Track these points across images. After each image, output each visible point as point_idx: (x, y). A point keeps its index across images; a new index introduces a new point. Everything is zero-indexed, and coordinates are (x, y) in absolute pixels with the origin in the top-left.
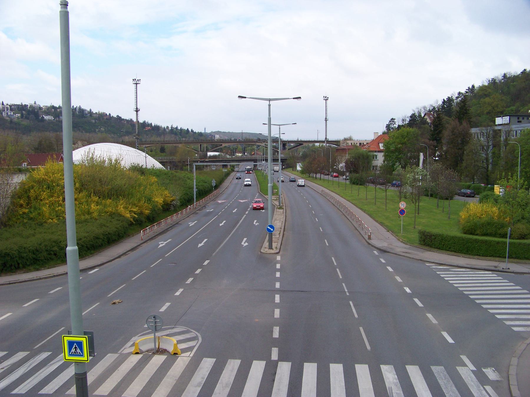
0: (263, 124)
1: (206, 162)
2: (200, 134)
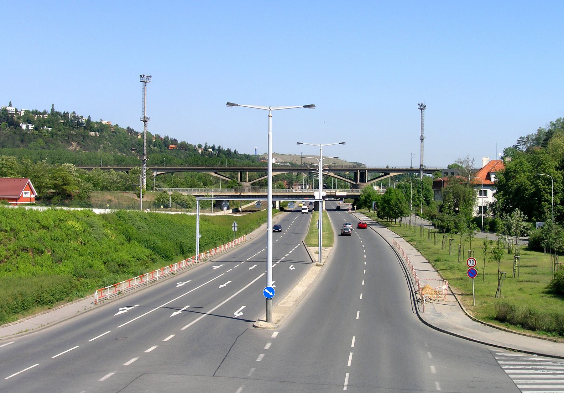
0: (297, 143)
1: (244, 197)
2: (247, 157)
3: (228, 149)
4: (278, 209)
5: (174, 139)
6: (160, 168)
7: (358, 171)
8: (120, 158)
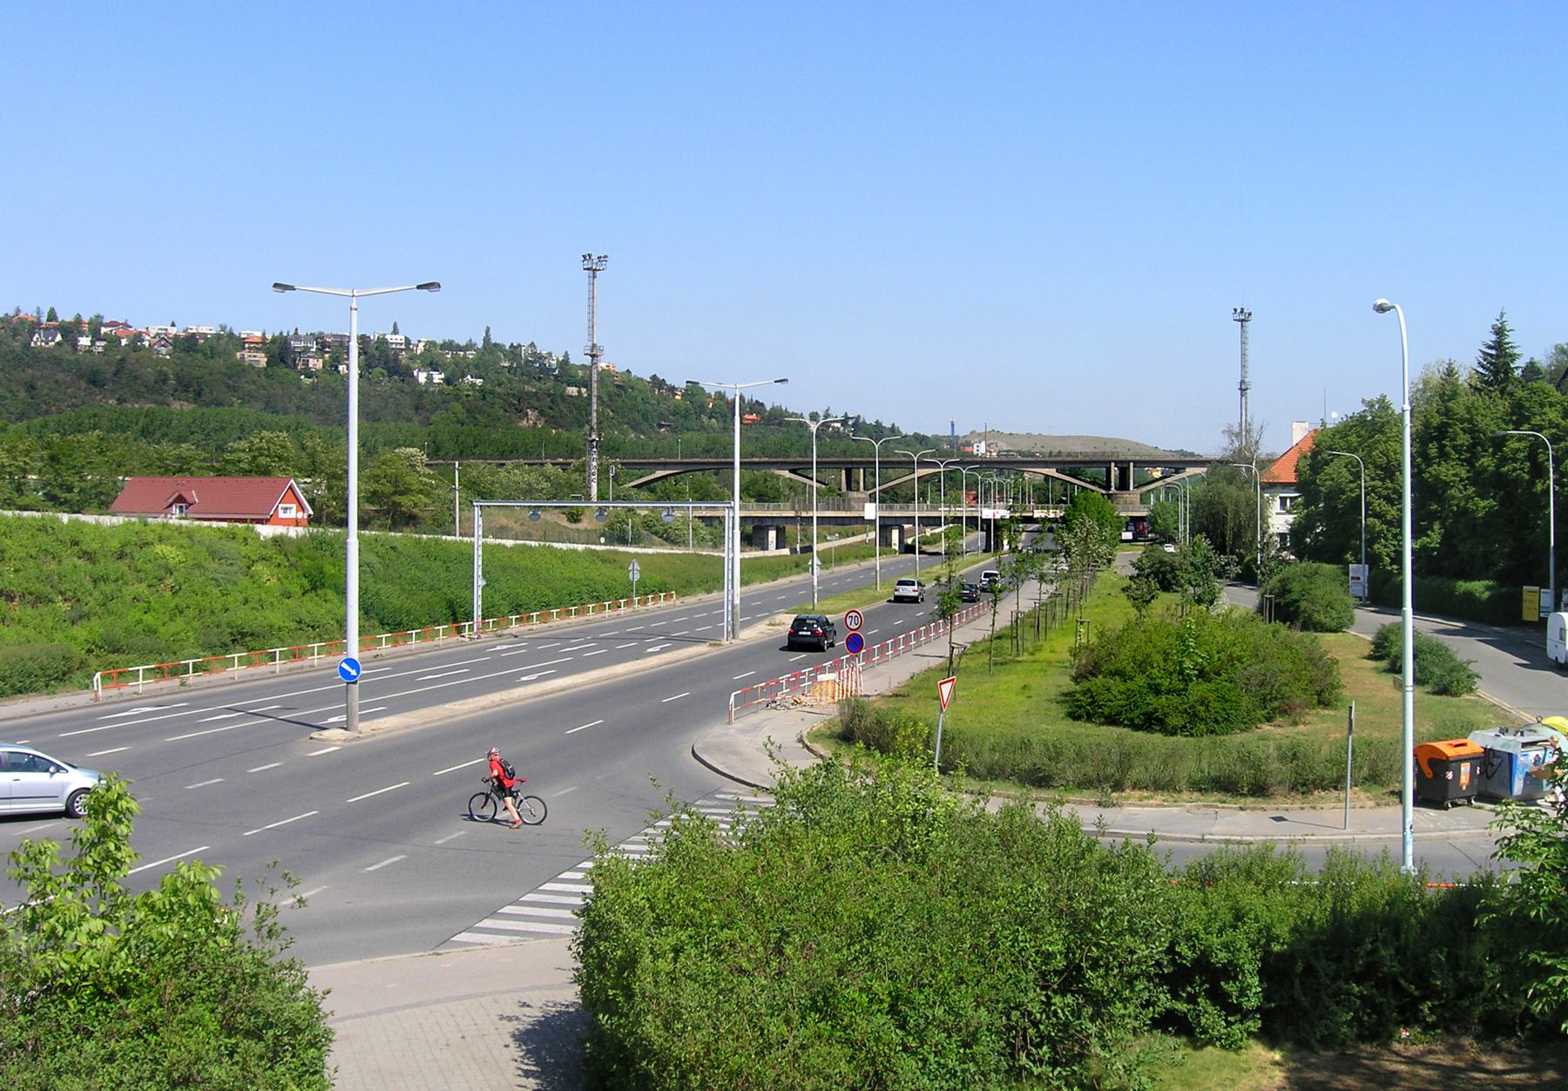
3: (877, 422)
4: (897, 548)
5: (757, 401)
8: (611, 444)
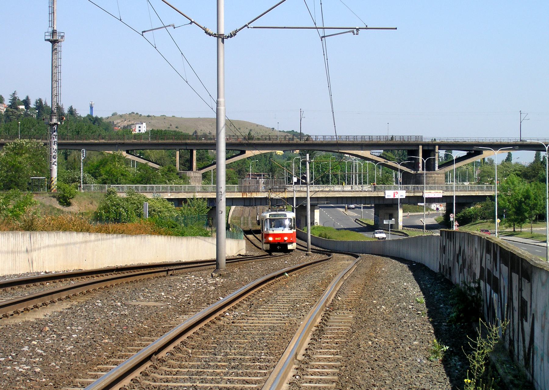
6: (96, 142)
7: (421, 147)
